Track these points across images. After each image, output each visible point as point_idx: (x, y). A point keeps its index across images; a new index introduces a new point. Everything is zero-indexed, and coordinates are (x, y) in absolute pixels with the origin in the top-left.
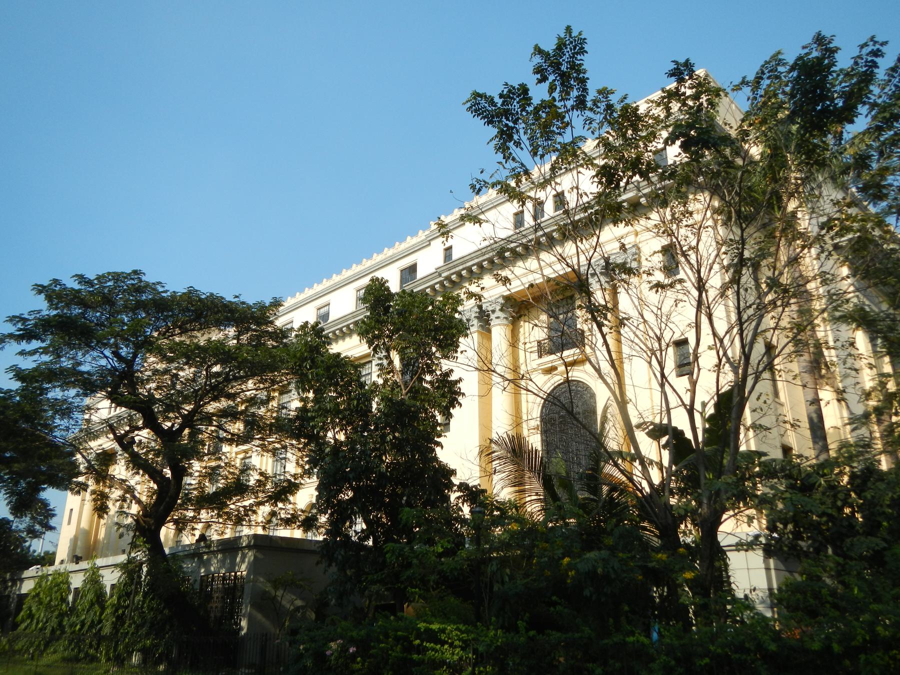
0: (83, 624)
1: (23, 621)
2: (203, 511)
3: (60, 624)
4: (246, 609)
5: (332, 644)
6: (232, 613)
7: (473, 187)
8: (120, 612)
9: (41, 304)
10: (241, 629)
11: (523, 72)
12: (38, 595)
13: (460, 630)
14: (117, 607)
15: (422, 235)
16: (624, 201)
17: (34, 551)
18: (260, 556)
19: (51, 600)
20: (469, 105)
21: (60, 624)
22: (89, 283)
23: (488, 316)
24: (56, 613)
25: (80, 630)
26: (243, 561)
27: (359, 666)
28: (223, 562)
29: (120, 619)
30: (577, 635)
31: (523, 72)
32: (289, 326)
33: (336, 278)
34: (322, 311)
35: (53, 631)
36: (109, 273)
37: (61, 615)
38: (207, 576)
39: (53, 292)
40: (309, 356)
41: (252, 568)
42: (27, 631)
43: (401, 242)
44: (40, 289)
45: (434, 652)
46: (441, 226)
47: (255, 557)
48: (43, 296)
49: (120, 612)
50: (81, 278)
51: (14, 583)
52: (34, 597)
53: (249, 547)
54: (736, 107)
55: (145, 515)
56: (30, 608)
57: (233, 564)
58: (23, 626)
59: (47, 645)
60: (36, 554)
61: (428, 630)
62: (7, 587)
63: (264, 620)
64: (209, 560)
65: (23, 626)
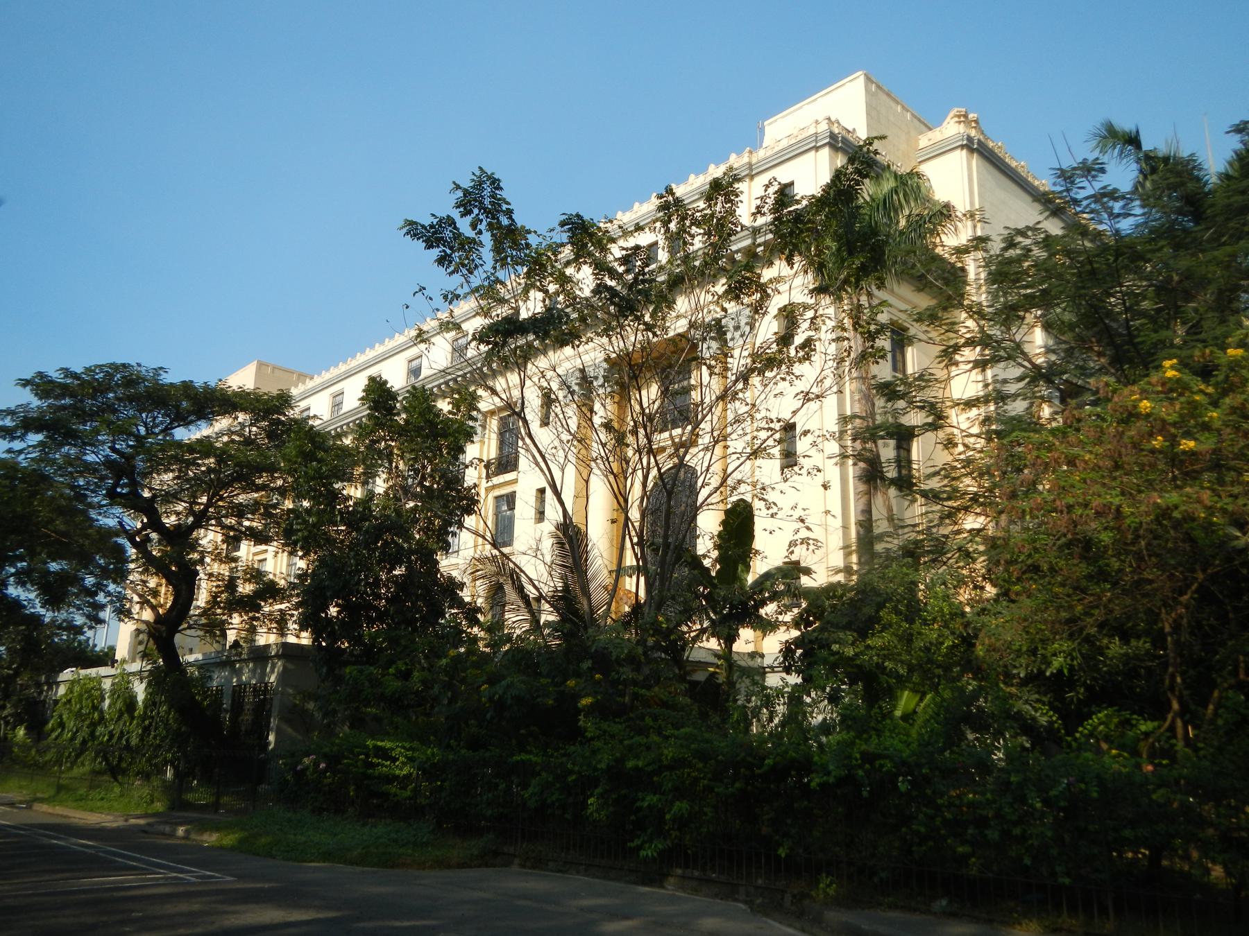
0: (111, 735)
1: (53, 730)
2: (235, 615)
3: (92, 734)
4: (274, 722)
5: (306, 760)
6: (260, 730)
7: (445, 297)
8: (147, 722)
9: (28, 398)
10: (269, 744)
11: (446, 206)
12: (69, 701)
13: (404, 747)
14: (144, 717)
15: (400, 339)
16: (737, 252)
17: (95, 646)
18: (290, 666)
19: (81, 708)
20: (405, 230)
21: (92, 734)
22: (75, 376)
23: (591, 382)
24: (87, 722)
25: (109, 740)
26: (272, 671)
27: (330, 780)
28: (253, 671)
29: (146, 730)
30: (487, 754)
31: (446, 206)
32: (305, 414)
33: (343, 368)
34: (415, 363)
35: (84, 742)
36: (97, 366)
37: (93, 725)
38: (239, 686)
39: (42, 385)
40: (311, 456)
41: (283, 677)
42: (59, 741)
43: (641, 203)
44: (25, 383)
45: (385, 767)
46: (421, 333)
47: (284, 667)
48: (28, 388)
49: (147, 722)
50: (67, 372)
51: (50, 688)
52: (65, 704)
53: (277, 656)
54: (913, 115)
55: (156, 621)
56: (60, 716)
57: (264, 674)
58: (54, 735)
59: (78, 756)
60: (97, 649)
61: (377, 748)
62: (41, 692)
63: (294, 734)
64: (241, 669)
65: (54, 735)
